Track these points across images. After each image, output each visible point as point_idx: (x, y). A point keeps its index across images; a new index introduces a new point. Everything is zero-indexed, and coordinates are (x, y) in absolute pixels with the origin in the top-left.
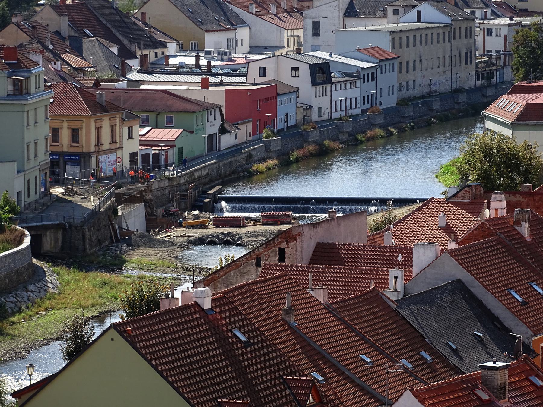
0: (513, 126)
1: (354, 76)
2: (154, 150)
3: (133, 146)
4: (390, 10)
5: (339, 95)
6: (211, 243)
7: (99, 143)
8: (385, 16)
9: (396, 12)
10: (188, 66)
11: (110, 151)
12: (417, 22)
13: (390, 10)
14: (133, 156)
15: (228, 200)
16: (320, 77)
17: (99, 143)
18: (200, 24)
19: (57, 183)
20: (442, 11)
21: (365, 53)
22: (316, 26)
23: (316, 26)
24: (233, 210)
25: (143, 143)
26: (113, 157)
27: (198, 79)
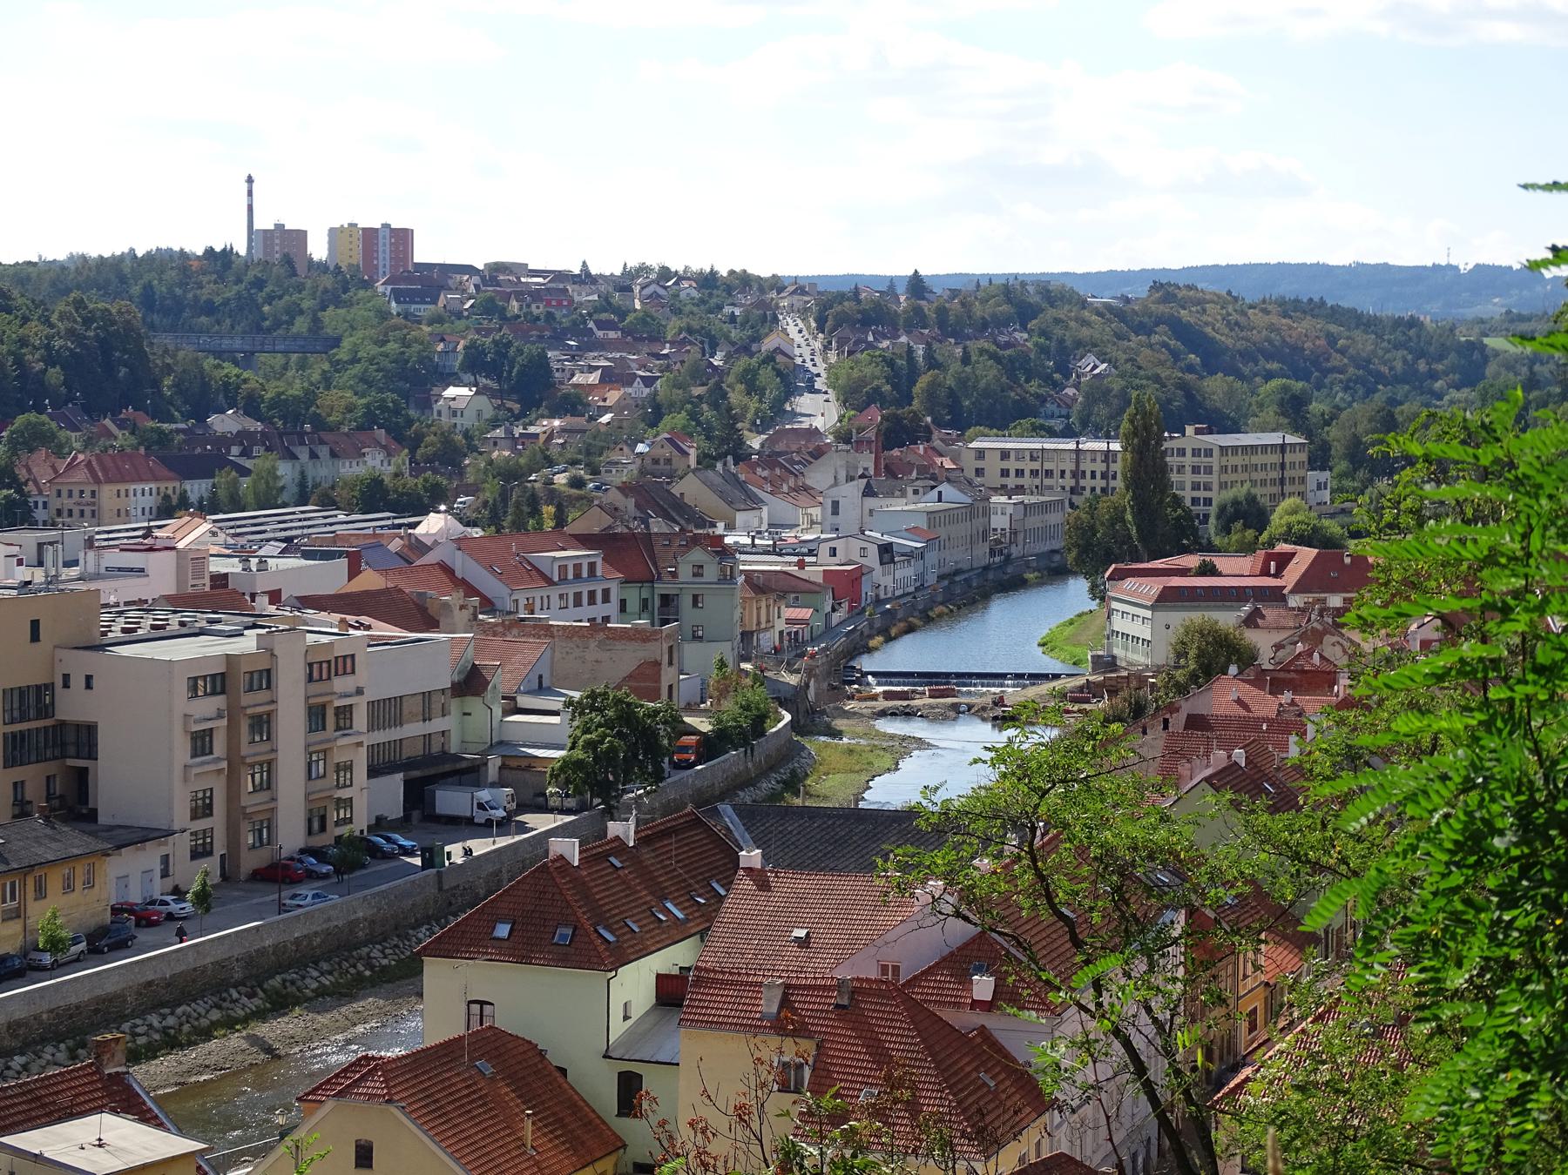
0: (1153, 608)
1: (910, 555)
2: (795, 628)
3: (780, 625)
4: (910, 490)
5: (899, 574)
6: (893, 714)
7: (759, 623)
8: (903, 494)
9: (916, 492)
10: (745, 546)
11: (766, 629)
12: (1261, 575)
13: (910, 490)
14: (781, 633)
15: (874, 674)
16: (886, 557)
17: (759, 623)
18: (730, 503)
19: (747, 659)
20: (961, 491)
21: (914, 532)
22: (835, 505)
23: (835, 505)
24: (879, 684)
25: (789, 621)
26: (768, 634)
27: (795, 559)
